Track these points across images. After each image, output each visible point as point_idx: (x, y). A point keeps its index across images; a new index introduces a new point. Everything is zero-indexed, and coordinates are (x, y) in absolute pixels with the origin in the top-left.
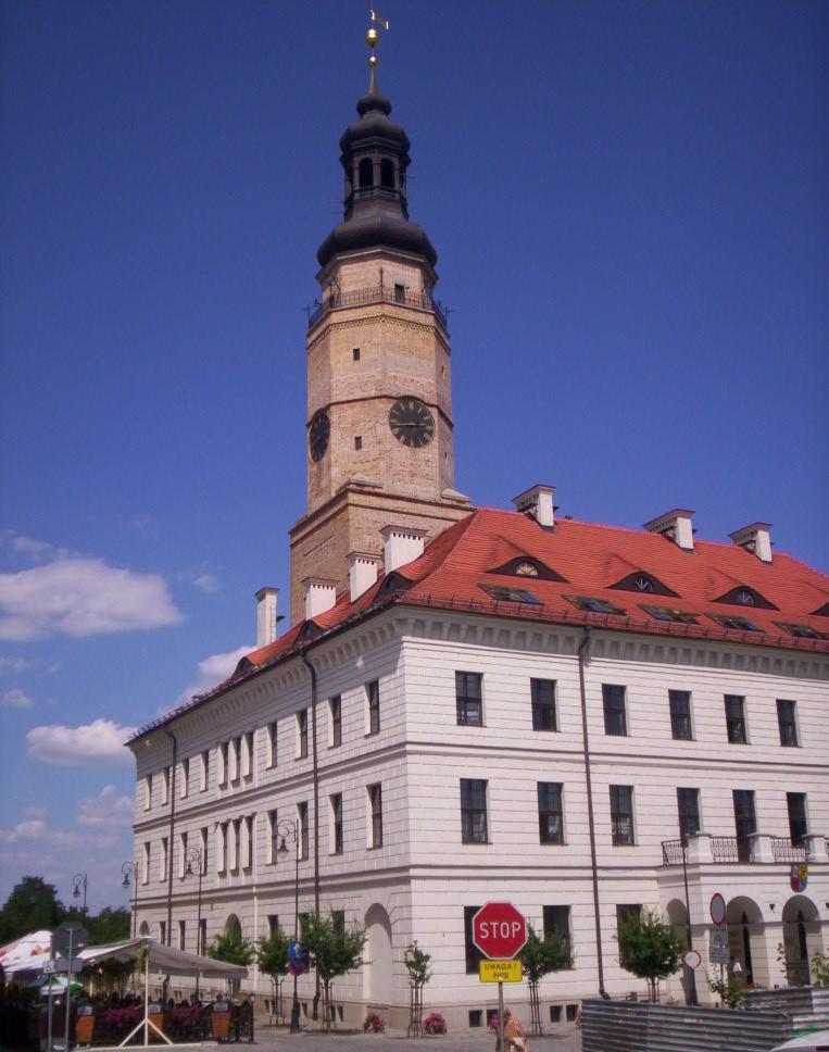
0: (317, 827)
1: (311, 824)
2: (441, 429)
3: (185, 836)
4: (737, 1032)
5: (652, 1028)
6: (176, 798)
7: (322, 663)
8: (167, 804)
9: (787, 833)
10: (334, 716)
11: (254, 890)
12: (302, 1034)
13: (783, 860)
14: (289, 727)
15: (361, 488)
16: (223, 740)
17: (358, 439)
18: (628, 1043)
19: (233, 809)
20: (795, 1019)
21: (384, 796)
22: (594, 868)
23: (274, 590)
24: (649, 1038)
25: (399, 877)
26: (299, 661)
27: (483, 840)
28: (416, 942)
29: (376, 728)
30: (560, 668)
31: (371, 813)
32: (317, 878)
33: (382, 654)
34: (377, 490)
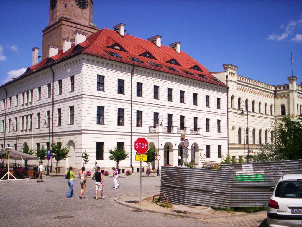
0: (53, 118)
1: (51, 117)
2: (90, 5)
3: (10, 120)
4: (217, 176)
5: (188, 174)
6: (7, 108)
7: (56, 70)
8: (4, 110)
9: (180, 126)
10: (71, 82)
11: (32, 136)
12: (50, 176)
13: (179, 133)
14: (45, 89)
15: (66, 20)
16: (23, 91)
17: (66, 4)
18: (179, 179)
19: (26, 112)
20: (236, 172)
21: (62, 112)
22: (131, 133)
23: (38, 48)
24: (187, 177)
25: (79, 133)
26: (49, 69)
27: (102, 123)
28: (85, 151)
29: (73, 89)
30: (126, 76)
31: (70, 115)
32: (53, 133)
33: (58, 75)
34: (71, 21)
